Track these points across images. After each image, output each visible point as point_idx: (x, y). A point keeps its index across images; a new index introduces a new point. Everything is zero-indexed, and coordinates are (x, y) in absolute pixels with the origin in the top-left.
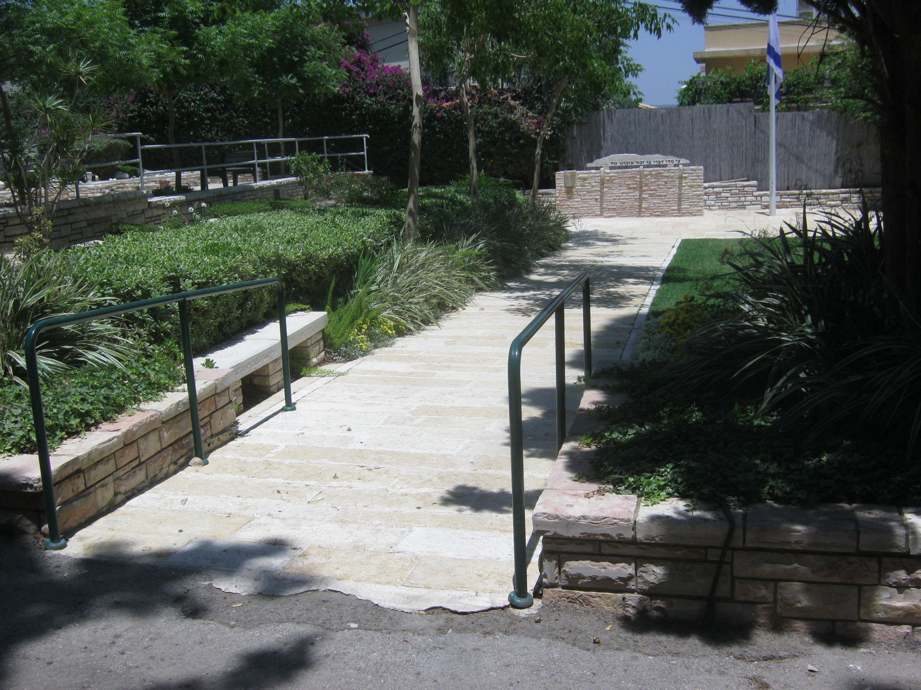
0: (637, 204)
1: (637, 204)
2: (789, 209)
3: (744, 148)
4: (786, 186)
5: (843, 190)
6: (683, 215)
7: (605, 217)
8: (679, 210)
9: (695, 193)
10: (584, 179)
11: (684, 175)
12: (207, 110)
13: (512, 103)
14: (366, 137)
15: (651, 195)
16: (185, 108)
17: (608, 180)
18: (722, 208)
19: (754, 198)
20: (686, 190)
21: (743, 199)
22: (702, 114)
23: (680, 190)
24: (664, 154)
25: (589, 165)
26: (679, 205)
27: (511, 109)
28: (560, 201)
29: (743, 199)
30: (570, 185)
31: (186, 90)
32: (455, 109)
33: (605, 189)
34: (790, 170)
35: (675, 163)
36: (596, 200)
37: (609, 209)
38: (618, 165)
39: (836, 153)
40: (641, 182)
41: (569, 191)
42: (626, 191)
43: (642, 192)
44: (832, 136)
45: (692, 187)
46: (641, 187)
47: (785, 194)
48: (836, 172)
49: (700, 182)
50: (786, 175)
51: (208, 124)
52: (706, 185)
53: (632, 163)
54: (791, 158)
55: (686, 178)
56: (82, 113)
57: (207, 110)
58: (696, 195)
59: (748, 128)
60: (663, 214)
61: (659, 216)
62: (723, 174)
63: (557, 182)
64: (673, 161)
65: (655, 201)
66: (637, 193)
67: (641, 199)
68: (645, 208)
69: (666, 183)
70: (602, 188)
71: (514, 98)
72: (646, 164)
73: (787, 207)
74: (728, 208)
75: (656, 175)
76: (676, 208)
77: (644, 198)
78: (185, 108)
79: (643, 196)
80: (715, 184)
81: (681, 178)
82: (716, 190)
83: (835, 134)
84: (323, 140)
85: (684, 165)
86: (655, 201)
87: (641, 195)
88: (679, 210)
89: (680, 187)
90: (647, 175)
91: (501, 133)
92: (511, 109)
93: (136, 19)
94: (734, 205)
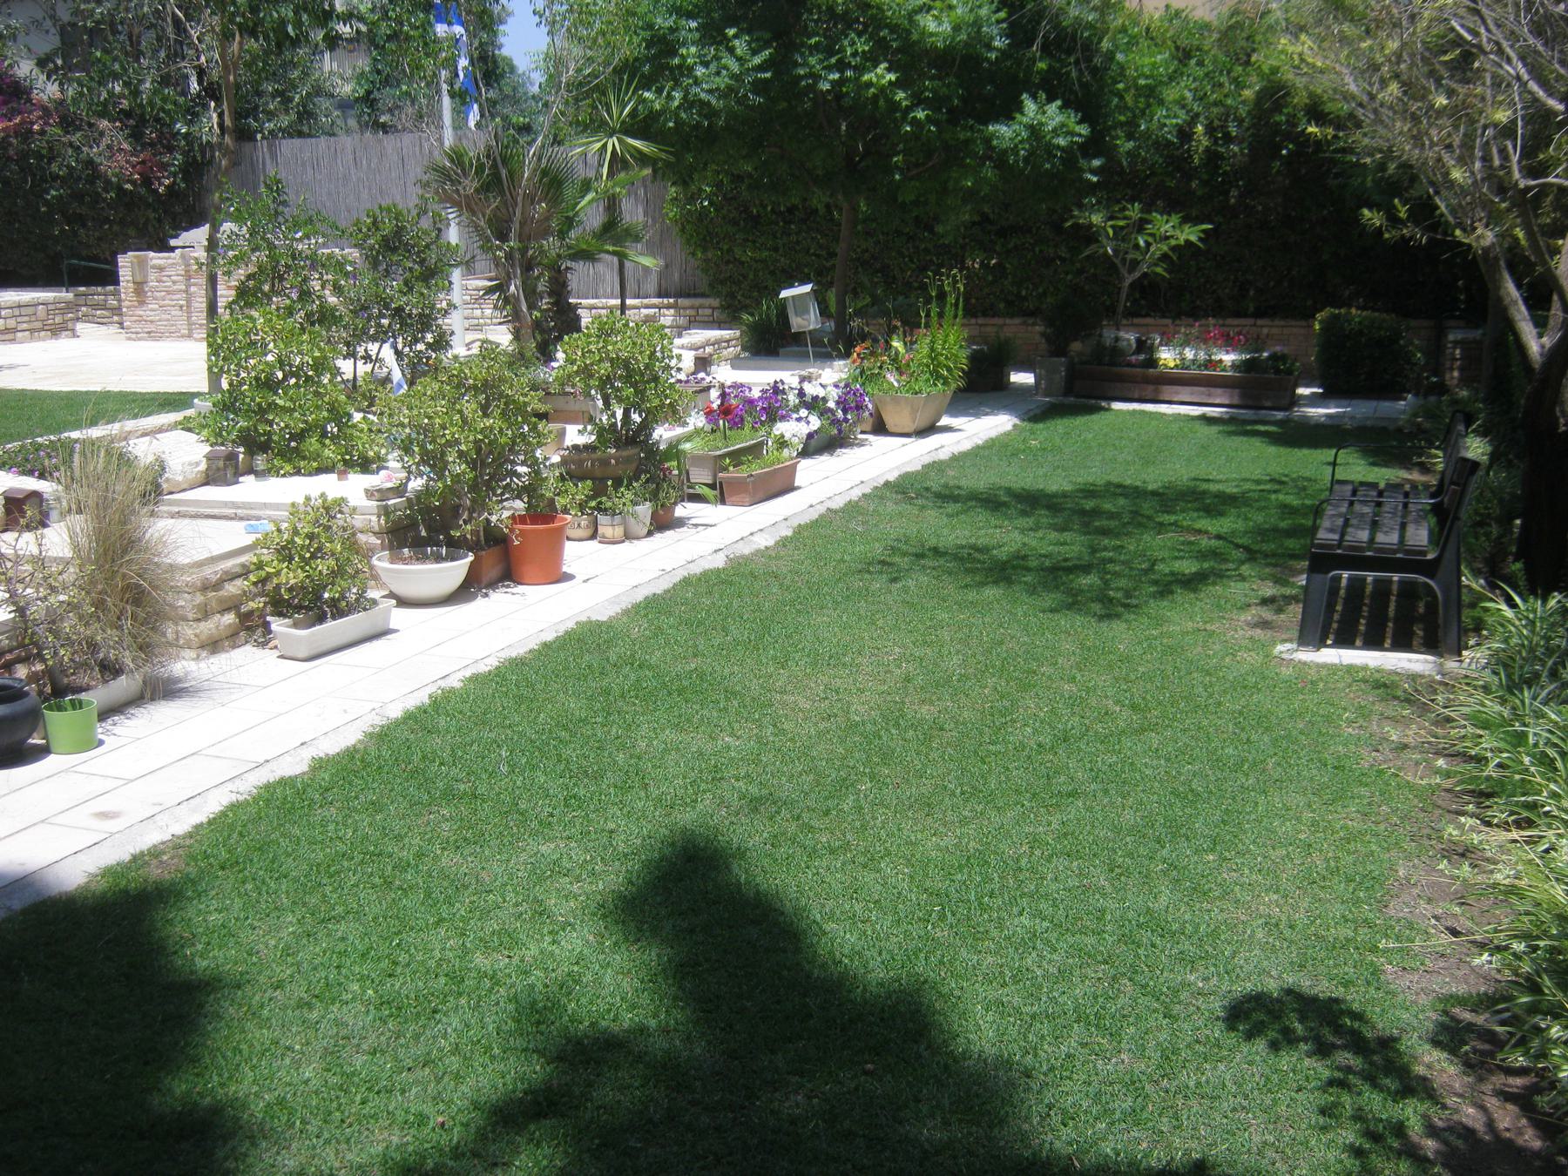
10: (161, 269)
21: (478, 313)
25: (173, 242)
29: (478, 313)
30: (138, 279)
31: (718, 89)
33: (193, 289)
36: (181, 307)
41: (140, 288)
56: (636, 59)
63: (121, 272)
93: (321, 597)
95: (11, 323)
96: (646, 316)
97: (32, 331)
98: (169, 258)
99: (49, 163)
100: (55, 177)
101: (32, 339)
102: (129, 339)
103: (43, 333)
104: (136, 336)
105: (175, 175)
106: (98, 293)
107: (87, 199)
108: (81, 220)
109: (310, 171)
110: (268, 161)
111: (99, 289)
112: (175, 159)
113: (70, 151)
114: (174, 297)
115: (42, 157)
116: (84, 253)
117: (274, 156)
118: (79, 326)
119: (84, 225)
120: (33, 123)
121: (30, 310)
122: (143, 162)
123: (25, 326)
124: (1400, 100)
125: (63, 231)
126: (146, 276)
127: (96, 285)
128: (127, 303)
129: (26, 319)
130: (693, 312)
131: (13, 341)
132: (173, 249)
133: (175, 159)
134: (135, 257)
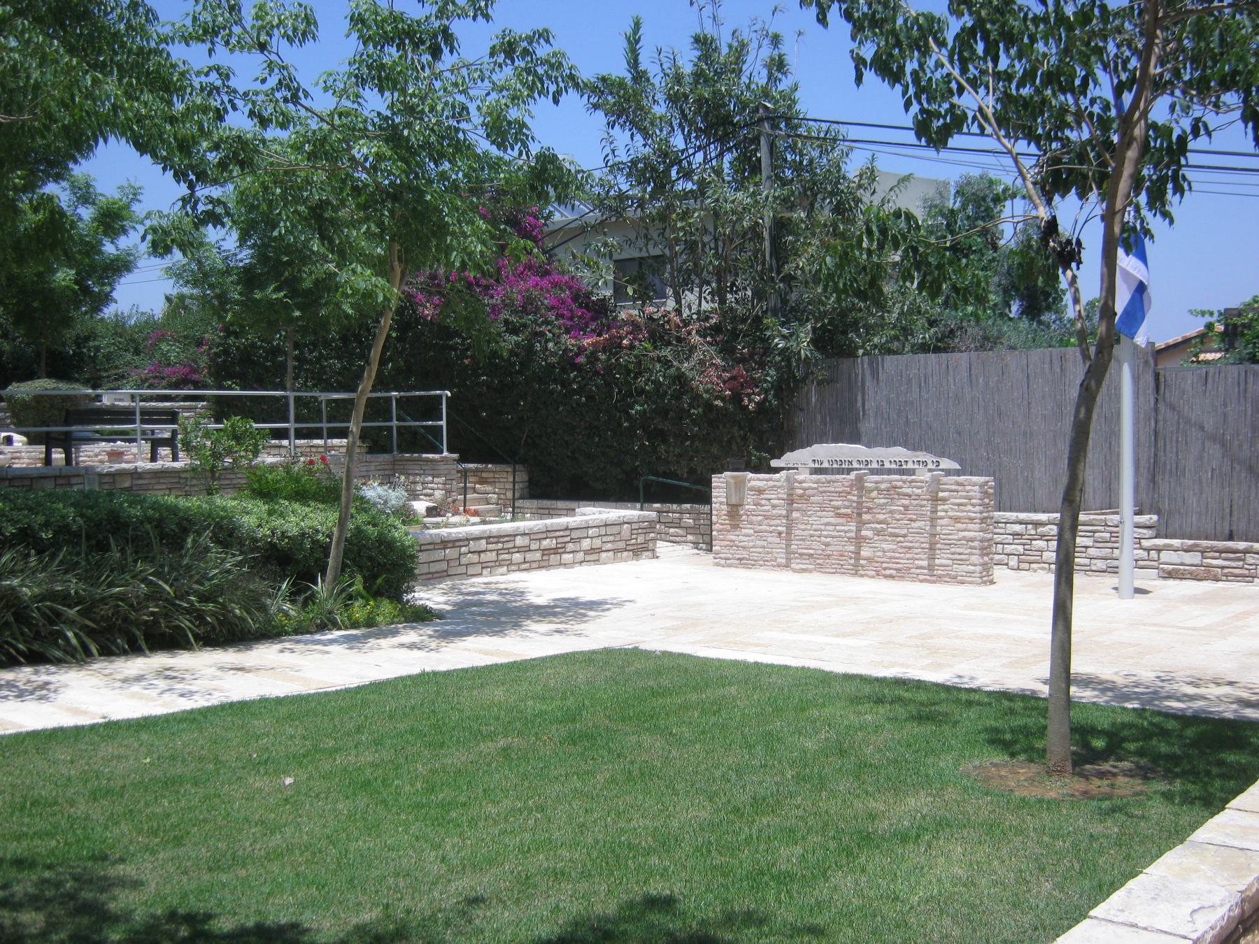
0: (852, 548)
1: (852, 548)
2: (1220, 584)
4: (1227, 532)
6: (939, 579)
7: (795, 571)
8: (931, 568)
10: (760, 491)
11: (941, 494)
13: (695, 339)
17: (801, 496)
19: (1144, 554)
23: (933, 526)
24: (914, 448)
25: (774, 463)
26: (932, 558)
30: (734, 501)
33: (795, 515)
34: (1236, 495)
35: (930, 466)
36: (780, 533)
37: (801, 554)
38: (826, 465)
41: (734, 511)
42: (833, 520)
43: (861, 524)
45: (957, 520)
46: (859, 515)
47: (1213, 550)
49: (974, 511)
50: (1226, 504)
53: (851, 463)
54: (1238, 467)
55: (944, 500)
58: (964, 538)
60: (901, 574)
61: (892, 577)
63: (715, 493)
65: (885, 546)
66: (852, 527)
67: (859, 540)
69: (906, 507)
70: (790, 512)
72: (875, 465)
76: (925, 563)
77: (865, 538)
79: (863, 533)
81: (935, 499)
84: (390, 399)
85: (948, 472)
86: (885, 546)
87: (859, 530)
88: (931, 568)
89: (933, 520)
94: (1100, 564)
95: (597, 543)
97: (615, 551)
98: (770, 480)
99: (636, 378)
100: (641, 392)
101: (615, 560)
102: (718, 565)
103: (625, 554)
104: (726, 563)
105: (766, 391)
106: (685, 513)
108: (661, 435)
109: (915, 388)
110: (868, 378)
111: (675, 506)
112: (768, 375)
113: (658, 366)
115: (628, 372)
116: (661, 469)
117: (875, 374)
118: (662, 547)
119: (664, 441)
120: (622, 338)
121: (615, 530)
122: (733, 378)
123: (609, 546)
125: (642, 446)
126: (742, 499)
127: (672, 502)
129: (611, 538)
131: (597, 561)
132: (777, 470)
133: (768, 375)
134: (733, 477)
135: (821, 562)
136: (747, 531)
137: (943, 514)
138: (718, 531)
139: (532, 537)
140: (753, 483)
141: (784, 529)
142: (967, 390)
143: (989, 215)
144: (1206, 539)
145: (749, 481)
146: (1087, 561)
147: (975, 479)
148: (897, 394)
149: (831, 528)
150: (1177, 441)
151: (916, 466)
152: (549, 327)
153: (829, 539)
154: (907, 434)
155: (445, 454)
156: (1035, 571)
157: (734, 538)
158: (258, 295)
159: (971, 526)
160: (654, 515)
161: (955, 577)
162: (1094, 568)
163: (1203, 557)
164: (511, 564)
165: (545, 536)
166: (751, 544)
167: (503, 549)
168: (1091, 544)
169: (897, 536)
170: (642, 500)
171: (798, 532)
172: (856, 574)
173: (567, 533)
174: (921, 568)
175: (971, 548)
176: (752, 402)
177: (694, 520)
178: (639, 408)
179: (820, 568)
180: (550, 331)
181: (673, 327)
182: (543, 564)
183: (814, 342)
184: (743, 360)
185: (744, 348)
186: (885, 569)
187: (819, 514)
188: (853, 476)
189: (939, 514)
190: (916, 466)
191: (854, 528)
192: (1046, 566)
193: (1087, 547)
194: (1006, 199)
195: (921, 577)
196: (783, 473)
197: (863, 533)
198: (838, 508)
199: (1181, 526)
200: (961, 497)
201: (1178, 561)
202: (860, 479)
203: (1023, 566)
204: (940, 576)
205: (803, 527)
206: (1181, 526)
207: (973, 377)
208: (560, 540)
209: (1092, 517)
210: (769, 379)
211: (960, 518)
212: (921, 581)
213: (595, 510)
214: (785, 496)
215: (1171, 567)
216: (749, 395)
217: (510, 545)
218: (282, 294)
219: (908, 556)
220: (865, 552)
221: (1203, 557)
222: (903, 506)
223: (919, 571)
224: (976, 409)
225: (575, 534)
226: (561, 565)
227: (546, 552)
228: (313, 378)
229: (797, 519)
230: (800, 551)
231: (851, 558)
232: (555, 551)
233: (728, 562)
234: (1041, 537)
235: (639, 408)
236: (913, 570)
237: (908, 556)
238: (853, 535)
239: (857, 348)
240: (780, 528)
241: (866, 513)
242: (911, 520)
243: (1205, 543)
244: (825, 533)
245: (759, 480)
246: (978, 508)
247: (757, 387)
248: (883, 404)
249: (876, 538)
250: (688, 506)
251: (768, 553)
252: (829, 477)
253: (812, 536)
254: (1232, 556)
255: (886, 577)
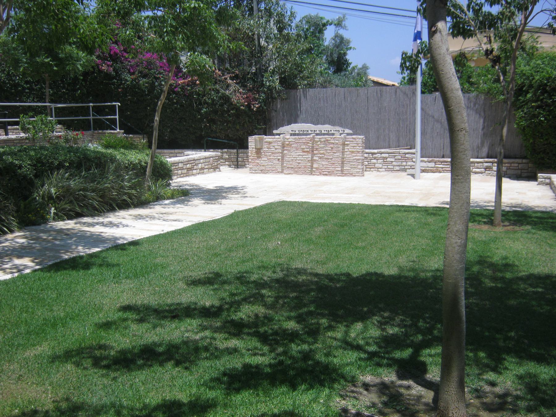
0: (310, 164)
2: (441, 174)
3: (408, 122)
5: (486, 160)
6: (346, 175)
7: (285, 174)
8: (342, 171)
9: (355, 158)
10: (270, 143)
11: (346, 143)
12: (27, 82)
13: (230, 81)
14: (118, 105)
15: (320, 158)
16: (13, 81)
17: (288, 144)
18: (388, 170)
20: (347, 155)
21: (404, 164)
22: (375, 94)
23: (343, 155)
24: (333, 124)
25: (275, 132)
26: (342, 167)
27: (228, 86)
28: (251, 159)
29: (404, 164)
30: (259, 147)
32: (188, 85)
33: (285, 152)
34: (445, 142)
35: (341, 132)
36: (279, 159)
37: (288, 167)
38: (297, 132)
39: (483, 129)
40: (313, 147)
41: (259, 151)
42: (301, 154)
43: (313, 155)
44: (480, 114)
45: (352, 152)
46: (313, 151)
47: (439, 161)
48: (482, 144)
49: (359, 149)
50: (442, 145)
51: (28, 92)
52: (367, 151)
55: (348, 145)
57: (27, 82)
58: (355, 159)
59: (411, 106)
61: (326, 175)
62: (391, 143)
64: (339, 131)
65: (324, 163)
66: (310, 156)
67: (312, 161)
68: (316, 168)
69: (332, 148)
71: (232, 78)
72: (318, 132)
73: (440, 172)
74: (392, 170)
75: (324, 141)
76: (340, 169)
77: (315, 160)
78: (13, 81)
79: (314, 158)
80: (383, 150)
81: (344, 145)
82: (383, 155)
83: (482, 114)
85: (348, 134)
86: (324, 163)
87: (312, 157)
88: (342, 171)
89: (343, 153)
90: (317, 142)
91: (222, 105)
92: (228, 86)
94: (397, 168)
96: (487, 166)
97: (209, 169)
98: (275, 138)
100: (206, 103)
101: (209, 172)
102: (251, 173)
107: (219, 113)
108: (213, 121)
110: (302, 98)
114: (275, 155)
117: (305, 96)
118: (221, 168)
121: (207, 160)
123: (207, 167)
124: (76, 79)
126: (262, 146)
128: (251, 157)
129: (207, 163)
130: (508, 165)
132: (273, 135)
135: (296, 170)
136: (264, 159)
137: (347, 150)
138: (251, 159)
139: (184, 163)
140: (267, 140)
141: (281, 158)
142: (343, 102)
143: (321, 31)
144: (438, 157)
145: (265, 139)
146: (392, 167)
147: (359, 137)
148: (315, 104)
149: (301, 157)
150: (424, 122)
151: (335, 132)
152: (162, 75)
153: (300, 161)
154: (318, 120)
155: (118, 130)
156: (372, 171)
157: (258, 162)
158: (38, 59)
159: (358, 154)
160: (219, 153)
161: (352, 174)
162: (395, 169)
163: (435, 164)
164: (178, 175)
165: (187, 163)
166: (266, 164)
167: (175, 169)
168: (394, 161)
169: (328, 159)
170: (205, 148)
171: (286, 159)
172: (311, 174)
173: (194, 162)
174: (338, 171)
175: (358, 163)
176: (256, 106)
177: (229, 156)
178: (205, 110)
179: (296, 172)
180: (162, 77)
181: (218, 75)
182: (187, 174)
183: (280, 82)
184: (250, 90)
185: (250, 85)
186: (323, 172)
187: (295, 151)
188: (311, 136)
189: (346, 150)
190: (335, 132)
191: (310, 157)
192: (377, 169)
193: (392, 162)
194: (327, 25)
195: (338, 174)
196: (281, 135)
197: (314, 158)
198: (304, 149)
199: (425, 153)
200: (354, 144)
201: (426, 166)
202: (313, 137)
203: (367, 169)
204: (346, 174)
205: (289, 157)
206: (425, 153)
207: (346, 98)
208: (192, 164)
209: (394, 151)
210: (262, 98)
211: (354, 151)
212: (338, 176)
213: (194, 152)
214: (281, 145)
215: (424, 168)
216: (253, 104)
217: (177, 167)
218: (49, 59)
219: (333, 166)
220: (315, 166)
221: (435, 164)
222: (331, 147)
223: (337, 172)
224: (347, 110)
225: (197, 162)
226: (193, 175)
227: (189, 169)
228: (37, 98)
229: (286, 153)
230: (287, 166)
231: (309, 168)
232: (189, 169)
233: (256, 171)
234: (375, 158)
235: (205, 110)
236: (335, 172)
237: (333, 166)
238: (310, 159)
239: (298, 86)
240: (279, 157)
241: (315, 150)
242: (334, 153)
243: (436, 159)
244: (298, 159)
245: (269, 138)
246: (361, 148)
247: (257, 101)
248: (309, 108)
249: (320, 160)
250: (226, 150)
251: (274, 167)
252: (300, 137)
253: (293, 160)
254: (446, 163)
255: (324, 175)
